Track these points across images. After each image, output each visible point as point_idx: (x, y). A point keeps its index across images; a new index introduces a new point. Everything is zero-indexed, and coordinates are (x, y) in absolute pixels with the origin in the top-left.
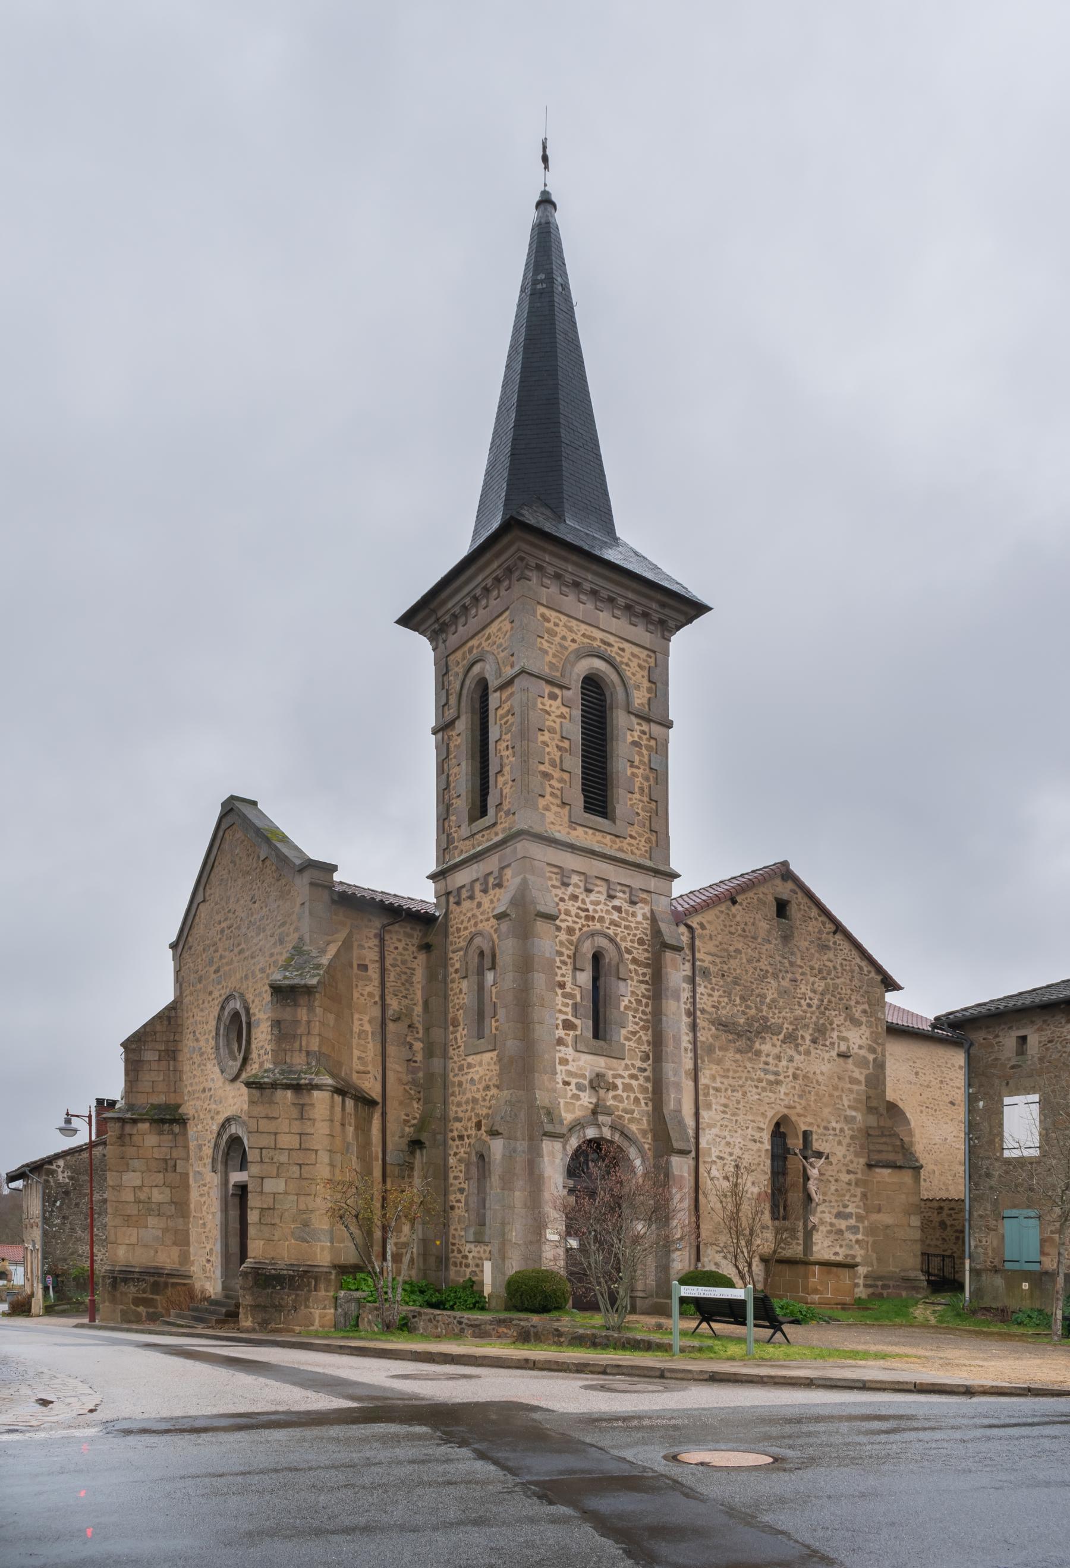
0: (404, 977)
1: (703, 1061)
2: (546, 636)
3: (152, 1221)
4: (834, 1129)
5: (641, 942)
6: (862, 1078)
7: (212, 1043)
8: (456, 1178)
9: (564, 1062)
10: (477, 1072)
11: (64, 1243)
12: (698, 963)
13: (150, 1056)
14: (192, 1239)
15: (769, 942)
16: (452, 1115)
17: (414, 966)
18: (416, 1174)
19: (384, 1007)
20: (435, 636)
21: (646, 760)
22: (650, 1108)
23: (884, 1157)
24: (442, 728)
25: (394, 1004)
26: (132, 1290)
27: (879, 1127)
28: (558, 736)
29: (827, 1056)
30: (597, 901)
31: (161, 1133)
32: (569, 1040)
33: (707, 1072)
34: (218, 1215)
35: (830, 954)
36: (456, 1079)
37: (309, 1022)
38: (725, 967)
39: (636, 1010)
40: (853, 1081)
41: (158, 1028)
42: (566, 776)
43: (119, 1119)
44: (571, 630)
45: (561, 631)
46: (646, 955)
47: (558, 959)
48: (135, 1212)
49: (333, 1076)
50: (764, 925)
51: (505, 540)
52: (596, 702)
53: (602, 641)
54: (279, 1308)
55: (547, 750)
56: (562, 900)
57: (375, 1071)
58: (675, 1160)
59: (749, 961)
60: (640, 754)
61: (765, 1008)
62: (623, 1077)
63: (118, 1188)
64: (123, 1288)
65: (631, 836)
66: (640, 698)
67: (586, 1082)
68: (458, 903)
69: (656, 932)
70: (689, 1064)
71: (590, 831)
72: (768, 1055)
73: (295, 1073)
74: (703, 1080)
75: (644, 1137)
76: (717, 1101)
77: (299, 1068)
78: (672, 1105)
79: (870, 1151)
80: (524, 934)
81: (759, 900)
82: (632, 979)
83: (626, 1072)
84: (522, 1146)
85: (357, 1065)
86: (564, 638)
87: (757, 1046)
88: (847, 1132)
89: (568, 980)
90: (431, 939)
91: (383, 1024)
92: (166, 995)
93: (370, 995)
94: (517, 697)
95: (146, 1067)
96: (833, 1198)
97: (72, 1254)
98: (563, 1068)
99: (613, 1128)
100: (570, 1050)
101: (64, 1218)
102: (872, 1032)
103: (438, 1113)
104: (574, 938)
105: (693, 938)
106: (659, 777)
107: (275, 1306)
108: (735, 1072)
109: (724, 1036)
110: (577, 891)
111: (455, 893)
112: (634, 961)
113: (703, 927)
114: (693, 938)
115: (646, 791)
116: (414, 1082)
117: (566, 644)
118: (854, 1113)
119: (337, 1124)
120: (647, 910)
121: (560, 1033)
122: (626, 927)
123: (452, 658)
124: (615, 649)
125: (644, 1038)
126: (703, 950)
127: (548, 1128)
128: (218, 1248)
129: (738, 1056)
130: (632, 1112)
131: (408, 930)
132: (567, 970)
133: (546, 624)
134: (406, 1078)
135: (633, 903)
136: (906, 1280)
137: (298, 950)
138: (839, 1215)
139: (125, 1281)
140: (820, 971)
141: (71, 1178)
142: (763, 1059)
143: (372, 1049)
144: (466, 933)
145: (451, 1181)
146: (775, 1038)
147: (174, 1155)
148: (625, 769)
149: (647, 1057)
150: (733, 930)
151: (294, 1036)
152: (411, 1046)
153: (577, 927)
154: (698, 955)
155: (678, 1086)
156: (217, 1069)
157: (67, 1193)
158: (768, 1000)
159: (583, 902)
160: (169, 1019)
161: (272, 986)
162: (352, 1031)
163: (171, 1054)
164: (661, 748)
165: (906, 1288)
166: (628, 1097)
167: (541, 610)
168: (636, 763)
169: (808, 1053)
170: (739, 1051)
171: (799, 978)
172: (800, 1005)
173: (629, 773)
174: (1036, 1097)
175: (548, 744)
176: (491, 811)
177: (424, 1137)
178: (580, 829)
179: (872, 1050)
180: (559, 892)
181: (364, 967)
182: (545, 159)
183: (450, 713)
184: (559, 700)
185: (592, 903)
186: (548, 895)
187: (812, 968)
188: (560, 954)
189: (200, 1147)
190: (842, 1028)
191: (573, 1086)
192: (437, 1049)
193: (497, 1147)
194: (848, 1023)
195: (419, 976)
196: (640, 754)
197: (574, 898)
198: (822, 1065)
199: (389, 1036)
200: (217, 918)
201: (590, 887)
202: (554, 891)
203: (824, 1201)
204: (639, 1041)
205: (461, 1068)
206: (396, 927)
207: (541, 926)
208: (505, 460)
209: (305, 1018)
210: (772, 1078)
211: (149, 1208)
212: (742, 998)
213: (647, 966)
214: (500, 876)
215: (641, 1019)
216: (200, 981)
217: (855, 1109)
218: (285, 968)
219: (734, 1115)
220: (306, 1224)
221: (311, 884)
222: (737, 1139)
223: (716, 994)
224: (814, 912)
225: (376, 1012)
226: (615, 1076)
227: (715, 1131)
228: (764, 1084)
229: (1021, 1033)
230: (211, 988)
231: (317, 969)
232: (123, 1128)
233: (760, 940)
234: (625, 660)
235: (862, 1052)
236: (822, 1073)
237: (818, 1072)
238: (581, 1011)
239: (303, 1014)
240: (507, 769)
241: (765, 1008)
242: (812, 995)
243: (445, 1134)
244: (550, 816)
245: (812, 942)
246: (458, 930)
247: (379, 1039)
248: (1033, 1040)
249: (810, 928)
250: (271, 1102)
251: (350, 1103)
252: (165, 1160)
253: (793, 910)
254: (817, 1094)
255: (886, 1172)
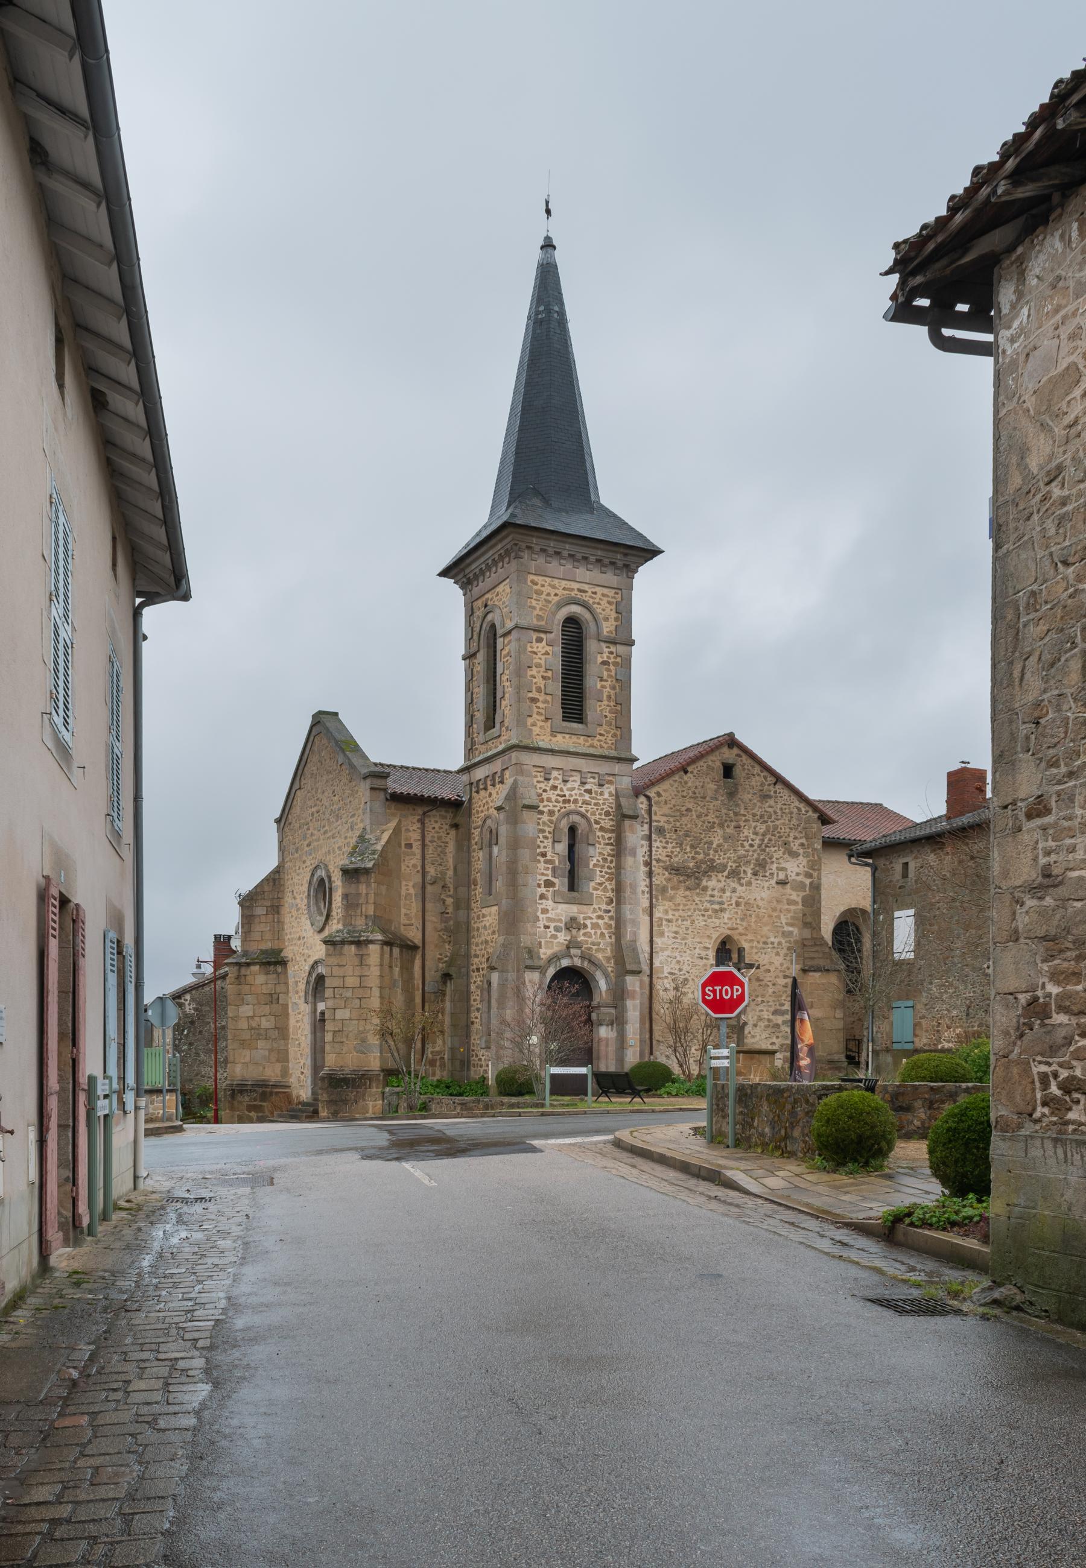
0: (439, 849)
1: (657, 900)
2: (535, 596)
3: (261, 1044)
4: (772, 943)
5: (607, 814)
6: (799, 900)
7: (305, 901)
8: (475, 1000)
9: (545, 911)
10: (488, 919)
11: (190, 1066)
12: (654, 824)
13: (260, 911)
14: (291, 1057)
15: (717, 799)
16: (473, 953)
17: (448, 840)
18: (448, 998)
19: (424, 873)
20: (466, 584)
21: (613, 674)
22: (613, 940)
23: (815, 963)
24: (469, 657)
25: (432, 871)
26: (246, 1099)
27: (813, 938)
28: (543, 669)
29: (766, 884)
30: (573, 789)
31: (267, 973)
32: (549, 895)
33: (661, 908)
34: (309, 1036)
35: (771, 802)
36: (475, 926)
37: (367, 894)
38: (678, 824)
39: (603, 867)
40: (790, 902)
41: (266, 888)
42: (549, 698)
43: (237, 964)
44: (554, 587)
45: (547, 589)
46: (612, 823)
47: (541, 835)
48: (248, 1037)
49: (383, 931)
50: (713, 786)
51: (504, 533)
52: (574, 636)
53: (580, 590)
54: (345, 1102)
55: (534, 680)
56: (545, 791)
57: (417, 923)
58: (629, 979)
59: (699, 816)
60: (609, 670)
61: (711, 852)
62: (591, 918)
63: (236, 1018)
64: (239, 1098)
65: (601, 734)
66: (608, 628)
67: (562, 925)
68: (477, 792)
69: (619, 806)
70: (646, 903)
71: (567, 736)
72: (713, 889)
73: (357, 932)
74: (657, 914)
75: (608, 962)
76: (668, 930)
77: (360, 928)
78: (628, 937)
79: (805, 958)
80: (514, 820)
81: (708, 767)
82: (600, 843)
83: (594, 917)
84: (511, 976)
85: (404, 920)
86: (548, 594)
87: (704, 883)
88: (784, 944)
89: (549, 850)
90: (459, 820)
91: (423, 888)
92: (273, 863)
93: (414, 866)
94: (513, 644)
95: (257, 920)
96: (771, 999)
97: (197, 1075)
98: (544, 916)
99: (582, 957)
100: (550, 902)
101: (191, 1044)
102: (808, 862)
103: (463, 952)
104: (554, 819)
105: (650, 806)
106: (623, 685)
107: (342, 1101)
108: (685, 905)
109: (675, 879)
110: (557, 783)
111: (475, 785)
112: (602, 829)
113: (659, 794)
114: (650, 806)
115: (613, 697)
116: (446, 929)
117: (550, 598)
118: (791, 929)
119: (386, 968)
120: (612, 789)
121: (543, 890)
122: (595, 804)
123: (475, 604)
124: (589, 594)
125: (609, 887)
126: (659, 813)
127: (529, 962)
128: (309, 1062)
129: (688, 893)
130: (599, 944)
131: (443, 813)
132: (548, 843)
133: (535, 587)
134: (440, 926)
135: (601, 785)
136: (831, 1062)
137: (362, 838)
138: (776, 1012)
139: (241, 1092)
140: (762, 816)
141: (196, 1009)
142: (709, 892)
143: (415, 907)
144: (482, 815)
145: (472, 1002)
146: (720, 875)
147: (278, 991)
148: (596, 685)
149: (611, 901)
150: (685, 794)
151: (357, 905)
152: (444, 901)
153: (556, 809)
154: (654, 818)
155: (634, 922)
156: (308, 922)
157: (192, 1023)
158: (714, 846)
159: (562, 790)
160: (275, 881)
161: (342, 870)
162: (400, 895)
163: (276, 909)
164: (626, 663)
165: (830, 1069)
166: (595, 933)
167: (531, 577)
168: (605, 678)
169: (749, 884)
170: (688, 888)
171: (742, 824)
172: (743, 846)
173: (599, 687)
174: (912, 912)
175: (535, 675)
176: (498, 725)
177: (453, 971)
178: (559, 736)
179: (808, 875)
180: (542, 785)
181: (409, 846)
182: (548, 212)
183: (473, 650)
184: (544, 642)
185: (568, 790)
186: (533, 787)
187: (754, 815)
188: (543, 831)
189: (297, 982)
190: (781, 861)
191: (552, 929)
192: (464, 904)
193: (495, 977)
194: (786, 856)
195: (451, 848)
196: (609, 670)
197: (554, 788)
198: (762, 892)
199: (428, 896)
200: (310, 803)
201: (566, 778)
202: (539, 785)
203: (763, 1001)
204: (605, 890)
205: (478, 918)
206: (434, 812)
207: (527, 815)
208: (511, 458)
209: (364, 892)
210: (717, 907)
211: (258, 1033)
212: (692, 847)
213: (612, 831)
214: (502, 776)
215: (607, 873)
216: (297, 850)
217: (792, 925)
218: (352, 854)
219: (683, 939)
220: (364, 1041)
221: (371, 789)
222: (686, 958)
223: (670, 845)
224: (757, 769)
225: (418, 878)
226: (585, 918)
227: (666, 953)
228: (710, 913)
229: (905, 860)
230: (304, 858)
231: (373, 854)
232: (239, 971)
233: (708, 799)
234: (597, 601)
235: (799, 878)
236: (762, 899)
237: (758, 898)
238: (559, 872)
239: (363, 889)
240: (507, 696)
241: (711, 852)
242: (754, 837)
243: (468, 968)
244: (536, 730)
245: (754, 794)
246: (478, 812)
247: (420, 899)
248: (912, 866)
249: (753, 783)
250: (341, 954)
251: (396, 951)
252: (271, 994)
253: (737, 771)
254: (757, 916)
255: (817, 975)
